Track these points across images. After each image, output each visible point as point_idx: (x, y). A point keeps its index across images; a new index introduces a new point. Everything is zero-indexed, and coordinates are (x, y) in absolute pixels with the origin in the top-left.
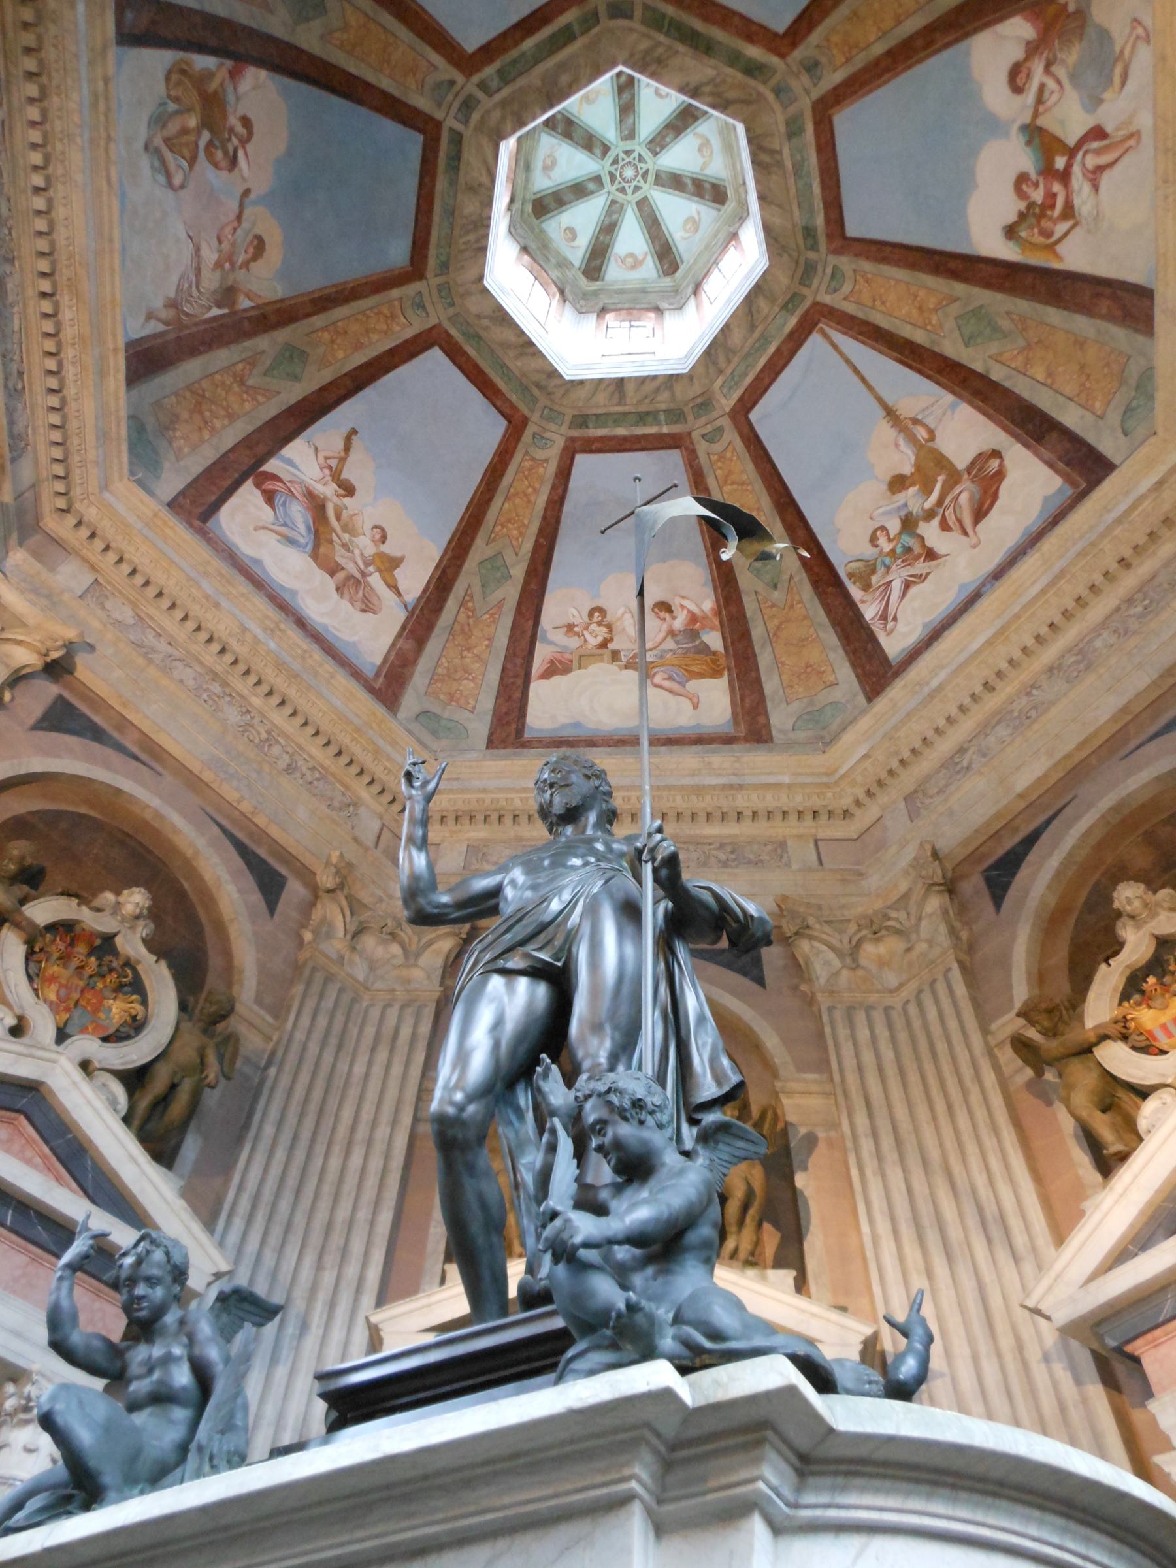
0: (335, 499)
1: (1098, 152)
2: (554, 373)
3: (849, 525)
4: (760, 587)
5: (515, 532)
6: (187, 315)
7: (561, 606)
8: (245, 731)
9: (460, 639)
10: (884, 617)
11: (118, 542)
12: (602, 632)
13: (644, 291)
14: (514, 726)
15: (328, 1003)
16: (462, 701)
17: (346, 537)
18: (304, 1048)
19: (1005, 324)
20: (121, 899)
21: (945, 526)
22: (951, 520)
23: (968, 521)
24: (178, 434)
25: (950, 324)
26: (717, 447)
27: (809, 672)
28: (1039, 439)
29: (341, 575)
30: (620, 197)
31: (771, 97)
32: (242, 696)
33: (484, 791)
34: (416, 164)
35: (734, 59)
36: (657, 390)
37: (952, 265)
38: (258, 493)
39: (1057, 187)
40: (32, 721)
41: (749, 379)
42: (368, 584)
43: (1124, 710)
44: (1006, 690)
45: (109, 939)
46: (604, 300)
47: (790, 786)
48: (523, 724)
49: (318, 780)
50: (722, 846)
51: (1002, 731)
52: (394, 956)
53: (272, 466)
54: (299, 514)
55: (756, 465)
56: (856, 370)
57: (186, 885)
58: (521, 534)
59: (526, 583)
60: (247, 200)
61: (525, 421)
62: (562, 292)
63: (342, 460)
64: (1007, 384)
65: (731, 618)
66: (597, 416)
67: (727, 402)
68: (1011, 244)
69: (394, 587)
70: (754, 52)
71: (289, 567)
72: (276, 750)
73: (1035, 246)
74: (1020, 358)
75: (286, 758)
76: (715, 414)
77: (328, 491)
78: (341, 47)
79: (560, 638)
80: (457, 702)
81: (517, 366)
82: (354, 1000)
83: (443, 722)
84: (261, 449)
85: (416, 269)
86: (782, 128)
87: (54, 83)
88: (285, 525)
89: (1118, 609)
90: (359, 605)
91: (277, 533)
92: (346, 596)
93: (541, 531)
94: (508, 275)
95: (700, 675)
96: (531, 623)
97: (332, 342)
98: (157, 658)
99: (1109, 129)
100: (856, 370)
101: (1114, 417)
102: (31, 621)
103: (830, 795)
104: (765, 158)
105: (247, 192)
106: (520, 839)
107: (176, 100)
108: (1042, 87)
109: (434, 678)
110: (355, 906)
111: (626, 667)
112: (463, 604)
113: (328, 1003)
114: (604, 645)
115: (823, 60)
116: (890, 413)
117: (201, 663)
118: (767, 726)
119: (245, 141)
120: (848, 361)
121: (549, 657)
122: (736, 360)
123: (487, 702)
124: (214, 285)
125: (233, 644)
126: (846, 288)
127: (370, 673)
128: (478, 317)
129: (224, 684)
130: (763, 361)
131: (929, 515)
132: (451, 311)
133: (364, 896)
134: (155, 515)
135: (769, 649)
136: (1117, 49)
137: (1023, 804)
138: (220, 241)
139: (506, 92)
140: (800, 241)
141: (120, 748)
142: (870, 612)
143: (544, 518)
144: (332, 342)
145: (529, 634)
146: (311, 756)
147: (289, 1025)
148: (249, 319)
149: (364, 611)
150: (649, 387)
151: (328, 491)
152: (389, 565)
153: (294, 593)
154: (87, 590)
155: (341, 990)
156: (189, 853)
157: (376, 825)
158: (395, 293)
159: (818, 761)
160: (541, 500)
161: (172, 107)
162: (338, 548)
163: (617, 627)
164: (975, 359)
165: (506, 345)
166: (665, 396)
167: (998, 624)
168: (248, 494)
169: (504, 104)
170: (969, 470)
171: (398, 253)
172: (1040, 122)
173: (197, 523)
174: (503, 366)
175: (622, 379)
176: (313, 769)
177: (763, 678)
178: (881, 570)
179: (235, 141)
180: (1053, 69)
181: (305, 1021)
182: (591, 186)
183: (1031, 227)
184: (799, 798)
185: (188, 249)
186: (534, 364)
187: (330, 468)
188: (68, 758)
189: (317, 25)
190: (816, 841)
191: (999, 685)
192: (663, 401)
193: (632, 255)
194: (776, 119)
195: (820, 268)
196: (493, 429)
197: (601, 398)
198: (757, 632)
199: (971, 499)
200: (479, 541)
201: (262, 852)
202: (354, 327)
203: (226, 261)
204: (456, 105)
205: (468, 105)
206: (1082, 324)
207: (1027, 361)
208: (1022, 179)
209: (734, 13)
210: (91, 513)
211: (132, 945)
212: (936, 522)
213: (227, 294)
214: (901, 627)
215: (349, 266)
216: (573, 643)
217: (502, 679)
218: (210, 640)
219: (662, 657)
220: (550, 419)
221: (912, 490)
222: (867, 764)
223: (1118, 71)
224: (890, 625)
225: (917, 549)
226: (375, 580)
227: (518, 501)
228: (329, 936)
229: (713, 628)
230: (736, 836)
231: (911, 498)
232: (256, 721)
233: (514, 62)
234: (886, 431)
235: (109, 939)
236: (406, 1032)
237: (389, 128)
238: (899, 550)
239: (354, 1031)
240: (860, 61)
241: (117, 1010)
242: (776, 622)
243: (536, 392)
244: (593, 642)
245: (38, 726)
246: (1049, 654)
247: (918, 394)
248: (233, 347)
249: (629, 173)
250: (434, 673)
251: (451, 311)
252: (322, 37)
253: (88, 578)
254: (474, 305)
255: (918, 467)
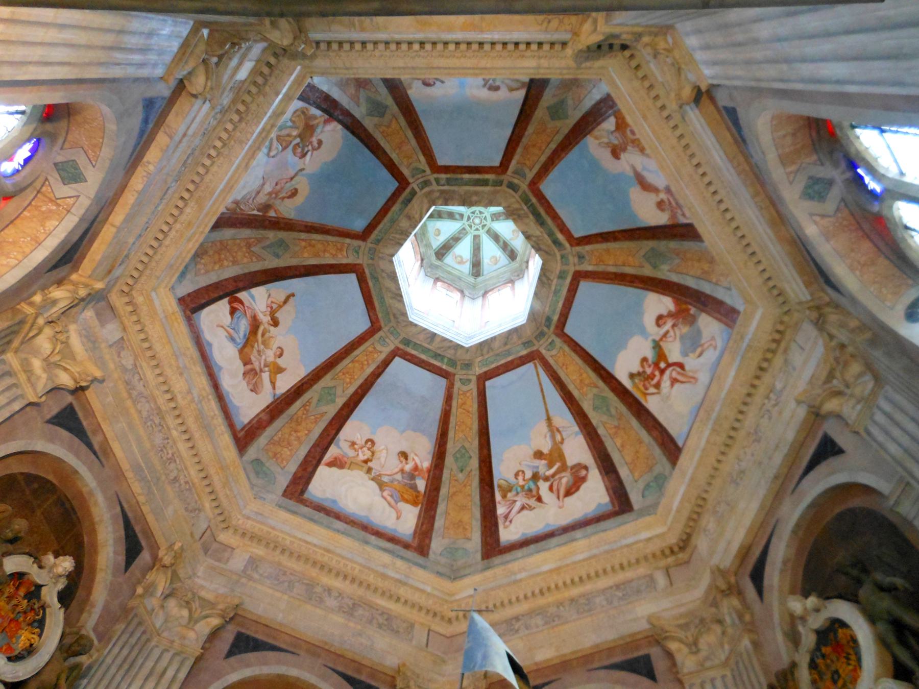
0: (266, 325)
1: (679, 373)
2: (405, 314)
3: (508, 463)
4: (455, 468)
5: (348, 380)
6: (241, 209)
7: (354, 430)
8: (162, 450)
9: (293, 425)
10: (506, 517)
11: (146, 319)
12: (368, 454)
13: (460, 278)
14: (301, 487)
15: (133, 641)
16: (279, 460)
17: (262, 347)
18: (109, 668)
19: (613, 411)
20: (57, 561)
21: (551, 488)
22: (555, 488)
23: (562, 492)
24: (203, 261)
25: (590, 396)
26: (465, 388)
27: (459, 525)
28: (607, 473)
29: (249, 367)
30: (468, 228)
31: (559, 257)
32: (169, 429)
33: (273, 528)
34: (389, 194)
35: (551, 234)
36: (449, 347)
37: (602, 372)
38: (228, 307)
39: (657, 373)
40: (48, 417)
41: (493, 366)
42: (261, 377)
43: (597, 646)
44: (550, 599)
45: (39, 587)
46: (440, 273)
47: (429, 594)
48: (306, 488)
49: (187, 490)
50: (382, 614)
51: (539, 621)
52: (182, 617)
53: (242, 295)
54: (244, 325)
55: (479, 406)
56: (542, 390)
57: (86, 539)
58: (351, 383)
59: (342, 409)
60: (300, 173)
61: (380, 329)
62: (422, 260)
63: (280, 307)
64: (604, 439)
65: (434, 478)
66: (416, 344)
67: (479, 370)
68: (630, 381)
69: (273, 383)
70: (560, 237)
71: (225, 354)
72: (173, 466)
73: (638, 388)
74: (614, 430)
75: (176, 471)
76: (470, 372)
77: (265, 319)
78: (382, 133)
79: (345, 446)
80: (277, 459)
81: (389, 301)
82: (148, 640)
83: (264, 469)
84: (241, 285)
85: (364, 235)
86: (558, 272)
87: (248, 118)
88: (234, 329)
89: (611, 587)
90: (251, 386)
91: (227, 332)
92: (247, 379)
93: (361, 386)
94: (406, 260)
95: (407, 501)
96: (334, 432)
97: (305, 247)
98: (135, 393)
99: (687, 368)
100: (542, 390)
101: (641, 485)
102: (79, 358)
103: (445, 607)
104: (544, 279)
105: (303, 169)
106: (279, 564)
107: (293, 122)
108: (667, 332)
109: (271, 442)
110: (175, 576)
111: (373, 479)
112: (304, 406)
113: (133, 641)
114: (366, 462)
115: (587, 257)
116: (549, 419)
117: (156, 403)
118: (429, 547)
119: (314, 149)
120: (540, 384)
121: (335, 455)
122: (491, 354)
123: (292, 467)
124: (263, 201)
125: (179, 397)
126: (554, 352)
127: (239, 427)
128: (383, 271)
129: (163, 418)
130: (503, 362)
131: (546, 479)
132: (370, 262)
133: (182, 573)
134: (173, 314)
135: (445, 502)
136: (703, 342)
137: (535, 668)
138: (276, 184)
139: (446, 188)
140: (544, 321)
141: (89, 445)
142: (501, 510)
143: (366, 380)
144: (305, 247)
145: (331, 436)
146: (189, 474)
147: (106, 652)
148: (270, 221)
149: (252, 391)
150: (446, 344)
151: (265, 319)
152: (278, 370)
153: (220, 368)
154: (115, 343)
155: (144, 632)
156: (97, 519)
157: (205, 526)
158: (348, 241)
159: (447, 585)
160: (369, 370)
161: (290, 124)
162: (255, 351)
163: (377, 455)
164: (595, 418)
165: (388, 289)
166: (452, 352)
167: (559, 564)
168: (222, 306)
169: (442, 192)
170: (572, 468)
171: (359, 225)
172: (661, 343)
173: (188, 313)
174: (382, 298)
175: (435, 334)
176: (187, 483)
177: (437, 518)
178: (514, 492)
179: (310, 147)
180: (676, 328)
181: (116, 650)
182: (457, 216)
183: (640, 380)
184: (430, 602)
185: (259, 182)
186: (397, 305)
187: (272, 308)
188: (59, 447)
189: (376, 120)
190: (429, 630)
191: (547, 594)
192: (450, 354)
193: (461, 257)
194: (557, 267)
195: (546, 337)
196: (363, 324)
197: (422, 337)
198: (443, 491)
199: (567, 483)
200: (328, 377)
201: (137, 529)
202: (320, 246)
203: (274, 194)
204: (421, 180)
205: (426, 183)
206: (644, 434)
207: (616, 433)
208: (644, 360)
209: (560, 218)
210: (140, 300)
211: (50, 596)
212: (548, 484)
213: (266, 207)
214: (512, 527)
215: (332, 219)
216: (351, 453)
217: (306, 456)
218: (167, 391)
219: (392, 482)
220: (392, 333)
221: (544, 462)
222: (471, 600)
223: (699, 350)
224: (507, 523)
225: (534, 493)
226: (266, 376)
227: (357, 365)
228: (152, 595)
229: (423, 478)
230: (391, 610)
231: (541, 465)
232: (169, 446)
233: (456, 179)
234: (543, 427)
235: (39, 587)
236: (170, 673)
237: (385, 173)
238: (526, 487)
239: (140, 661)
240: (600, 268)
241: (24, 638)
242: (455, 489)
243: (392, 317)
244: (362, 457)
245: (49, 422)
246: (575, 591)
247: (564, 418)
248: (254, 231)
249: (477, 221)
250: (272, 438)
251: (370, 262)
252: (376, 125)
253: (117, 335)
254: (383, 264)
255: (551, 451)
